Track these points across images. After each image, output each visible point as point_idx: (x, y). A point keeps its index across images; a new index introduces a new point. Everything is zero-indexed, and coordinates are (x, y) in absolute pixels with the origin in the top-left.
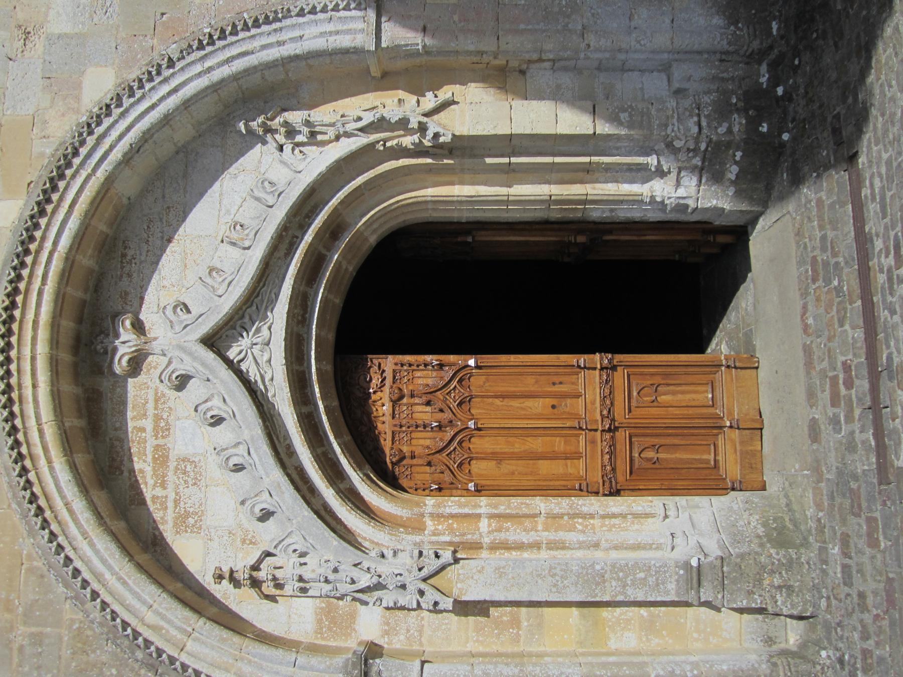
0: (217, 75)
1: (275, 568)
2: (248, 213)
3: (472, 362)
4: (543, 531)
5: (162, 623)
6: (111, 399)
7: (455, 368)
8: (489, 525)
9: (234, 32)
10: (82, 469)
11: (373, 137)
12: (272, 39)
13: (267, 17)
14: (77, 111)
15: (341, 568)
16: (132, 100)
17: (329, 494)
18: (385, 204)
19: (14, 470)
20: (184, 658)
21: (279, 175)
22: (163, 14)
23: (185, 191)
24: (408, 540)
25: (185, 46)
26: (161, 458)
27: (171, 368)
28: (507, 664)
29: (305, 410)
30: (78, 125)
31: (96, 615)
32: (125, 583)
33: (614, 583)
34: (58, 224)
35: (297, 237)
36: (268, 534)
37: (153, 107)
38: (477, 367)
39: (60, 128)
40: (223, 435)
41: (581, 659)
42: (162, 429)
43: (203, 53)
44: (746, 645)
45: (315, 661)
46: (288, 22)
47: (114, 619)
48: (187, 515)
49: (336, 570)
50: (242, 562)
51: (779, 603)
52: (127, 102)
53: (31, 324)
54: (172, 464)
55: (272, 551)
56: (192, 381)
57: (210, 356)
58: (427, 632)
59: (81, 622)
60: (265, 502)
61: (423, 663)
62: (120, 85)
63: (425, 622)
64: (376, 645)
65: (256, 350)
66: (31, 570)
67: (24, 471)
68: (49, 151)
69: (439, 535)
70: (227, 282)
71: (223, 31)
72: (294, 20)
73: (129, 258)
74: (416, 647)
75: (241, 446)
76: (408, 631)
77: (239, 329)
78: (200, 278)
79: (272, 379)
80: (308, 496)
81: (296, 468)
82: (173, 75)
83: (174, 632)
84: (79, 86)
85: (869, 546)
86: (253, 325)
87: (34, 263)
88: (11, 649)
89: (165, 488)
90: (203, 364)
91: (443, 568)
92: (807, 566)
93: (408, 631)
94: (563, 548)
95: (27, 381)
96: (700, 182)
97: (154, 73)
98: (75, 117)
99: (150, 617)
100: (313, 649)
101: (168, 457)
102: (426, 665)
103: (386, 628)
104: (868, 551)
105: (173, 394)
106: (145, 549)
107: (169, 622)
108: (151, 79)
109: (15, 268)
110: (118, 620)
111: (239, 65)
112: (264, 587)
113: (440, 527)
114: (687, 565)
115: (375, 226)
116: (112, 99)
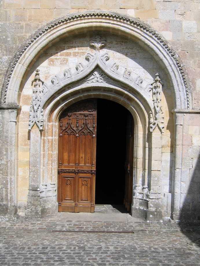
0: (169, 68)
1: (39, 85)
2: (134, 76)
3: (94, 135)
4: (48, 153)
5: (26, 58)
6: (83, 40)
7: (93, 131)
8: (50, 139)
9: (182, 73)
10: (64, 35)
11: (153, 111)
12: (179, 83)
13: (185, 82)
14: (159, 30)
15: (39, 102)
16: (162, 45)
17: (58, 98)
18: (137, 113)
19: (63, 19)
20: (17, 64)
21: (144, 85)
22: (188, 52)
23: (140, 58)
24: (45, 118)
25: (177, 59)
26: (68, 55)
27: (91, 56)
28: (15, 142)
29: (81, 91)
30: (155, 31)
31: (28, 42)
32: (35, 48)
33: (34, 169)
34: (128, 27)
35: (127, 89)
36: (48, 83)
37: (160, 51)
38: (93, 137)
39: (154, 26)
40: (73, 71)
41: (16, 161)
42: (75, 55)
43: (176, 64)
44: (19, 202)
45: (16, 96)
46: (184, 87)
47: (26, 46)
48: (53, 62)
49: (38, 100)
50: (41, 77)
51: (28, 209)
52: (162, 44)
53: (101, 21)
54: (66, 57)
55: (44, 84)
56: (88, 62)
57: (93, 67)
58: (23, 123)
59: (26, 38)
60: (56, 82)
61: (16, 122)
62: (166, 42)
63: (26, 122)
64: (21, 110)
65: (96, 79)
66: (38, 25)
67: (63, 22)
68: (148, 23)
69: (47, 126)
70: (114, 71)
71: (182, 70)
72: (185, 89)
73: (122, 43)
74: (20, 120)
75: (70, 75)
76: (24, 118)
77: (101, 74)
78: (115, 63)
79: (88, 83)
80: (58, 93)
81: (65, 89)
82: (169, 56)
83: (24, 61)
84: (167, 30)
85: (39, 228)
86: (103, 78)
87: (117, 21)
88: (20, 21)
89: (60, 56)
90: (92, 65)
91: (38, 127)
92: (37, 217)
93: (24, 118)
94: (43, 157)
95: (86, 21)
96: (140, 199)
97: (170, 51)
98: (158, 30)
99: (27, 55)
100: (19, 95)
101: (68, 56)
102: (15, 123)
103: (25, 113)
104: (38, 228)
105: (84, 57)
106: (44, 51)
107: (26, 60)
108: (168, 50)
109: (115, 16)
110: (26, 48)
111: (172, 74)
112: (34, 82)
113: (50, 126)
114: (38, 188)
115: (131, 110)
116: (162, 40)
